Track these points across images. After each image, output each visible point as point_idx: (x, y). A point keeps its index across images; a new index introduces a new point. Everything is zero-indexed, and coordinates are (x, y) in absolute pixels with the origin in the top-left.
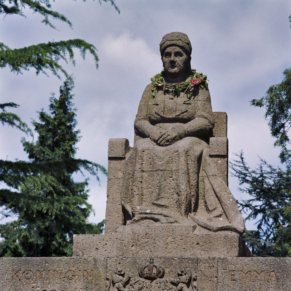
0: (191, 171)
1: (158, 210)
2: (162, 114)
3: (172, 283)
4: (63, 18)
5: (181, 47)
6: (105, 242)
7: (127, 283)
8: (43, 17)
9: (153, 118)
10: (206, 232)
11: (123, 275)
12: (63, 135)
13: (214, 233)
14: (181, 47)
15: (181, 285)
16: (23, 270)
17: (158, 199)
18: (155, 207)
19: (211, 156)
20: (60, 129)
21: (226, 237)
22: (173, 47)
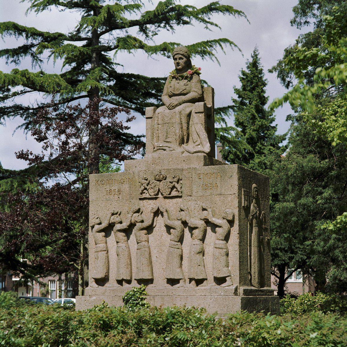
0: (183, 122)
1: (167, 144)
2: (173, 92)
3: (170, 182)
4: (216, 25)
5: (182, 55)
7: (149, 184)
8: (205, 26)
9: (169, 94)
11: (147, 180)
12: (256, 83)
13: (192, 155)
14: (182, 55)
15: (174, 183)
16: (100, 180)
17: (166, 139)
18: (165, 143)
19: (196, 113)
20: (255, 79)
21: (197, 156)
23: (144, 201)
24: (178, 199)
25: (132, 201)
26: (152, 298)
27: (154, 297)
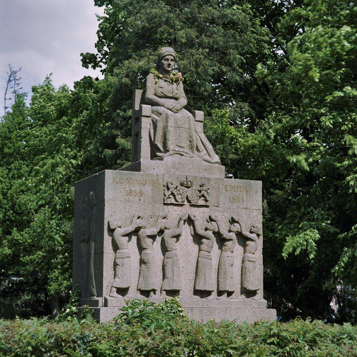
6: (158, 165)
10: (208, 164)
22: (170, 56)
23: (169, 207)
24: (205, 209)
25: (155, 205)
26: (189, 310)
27: (191, 310)
